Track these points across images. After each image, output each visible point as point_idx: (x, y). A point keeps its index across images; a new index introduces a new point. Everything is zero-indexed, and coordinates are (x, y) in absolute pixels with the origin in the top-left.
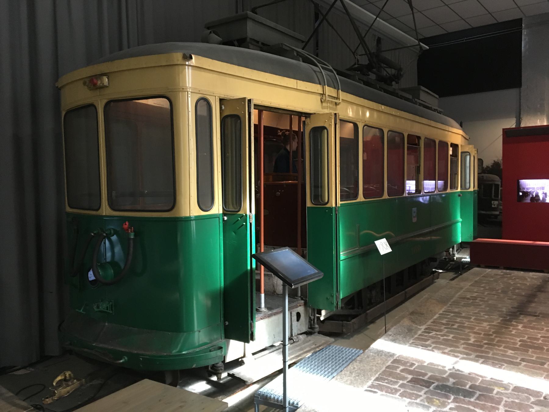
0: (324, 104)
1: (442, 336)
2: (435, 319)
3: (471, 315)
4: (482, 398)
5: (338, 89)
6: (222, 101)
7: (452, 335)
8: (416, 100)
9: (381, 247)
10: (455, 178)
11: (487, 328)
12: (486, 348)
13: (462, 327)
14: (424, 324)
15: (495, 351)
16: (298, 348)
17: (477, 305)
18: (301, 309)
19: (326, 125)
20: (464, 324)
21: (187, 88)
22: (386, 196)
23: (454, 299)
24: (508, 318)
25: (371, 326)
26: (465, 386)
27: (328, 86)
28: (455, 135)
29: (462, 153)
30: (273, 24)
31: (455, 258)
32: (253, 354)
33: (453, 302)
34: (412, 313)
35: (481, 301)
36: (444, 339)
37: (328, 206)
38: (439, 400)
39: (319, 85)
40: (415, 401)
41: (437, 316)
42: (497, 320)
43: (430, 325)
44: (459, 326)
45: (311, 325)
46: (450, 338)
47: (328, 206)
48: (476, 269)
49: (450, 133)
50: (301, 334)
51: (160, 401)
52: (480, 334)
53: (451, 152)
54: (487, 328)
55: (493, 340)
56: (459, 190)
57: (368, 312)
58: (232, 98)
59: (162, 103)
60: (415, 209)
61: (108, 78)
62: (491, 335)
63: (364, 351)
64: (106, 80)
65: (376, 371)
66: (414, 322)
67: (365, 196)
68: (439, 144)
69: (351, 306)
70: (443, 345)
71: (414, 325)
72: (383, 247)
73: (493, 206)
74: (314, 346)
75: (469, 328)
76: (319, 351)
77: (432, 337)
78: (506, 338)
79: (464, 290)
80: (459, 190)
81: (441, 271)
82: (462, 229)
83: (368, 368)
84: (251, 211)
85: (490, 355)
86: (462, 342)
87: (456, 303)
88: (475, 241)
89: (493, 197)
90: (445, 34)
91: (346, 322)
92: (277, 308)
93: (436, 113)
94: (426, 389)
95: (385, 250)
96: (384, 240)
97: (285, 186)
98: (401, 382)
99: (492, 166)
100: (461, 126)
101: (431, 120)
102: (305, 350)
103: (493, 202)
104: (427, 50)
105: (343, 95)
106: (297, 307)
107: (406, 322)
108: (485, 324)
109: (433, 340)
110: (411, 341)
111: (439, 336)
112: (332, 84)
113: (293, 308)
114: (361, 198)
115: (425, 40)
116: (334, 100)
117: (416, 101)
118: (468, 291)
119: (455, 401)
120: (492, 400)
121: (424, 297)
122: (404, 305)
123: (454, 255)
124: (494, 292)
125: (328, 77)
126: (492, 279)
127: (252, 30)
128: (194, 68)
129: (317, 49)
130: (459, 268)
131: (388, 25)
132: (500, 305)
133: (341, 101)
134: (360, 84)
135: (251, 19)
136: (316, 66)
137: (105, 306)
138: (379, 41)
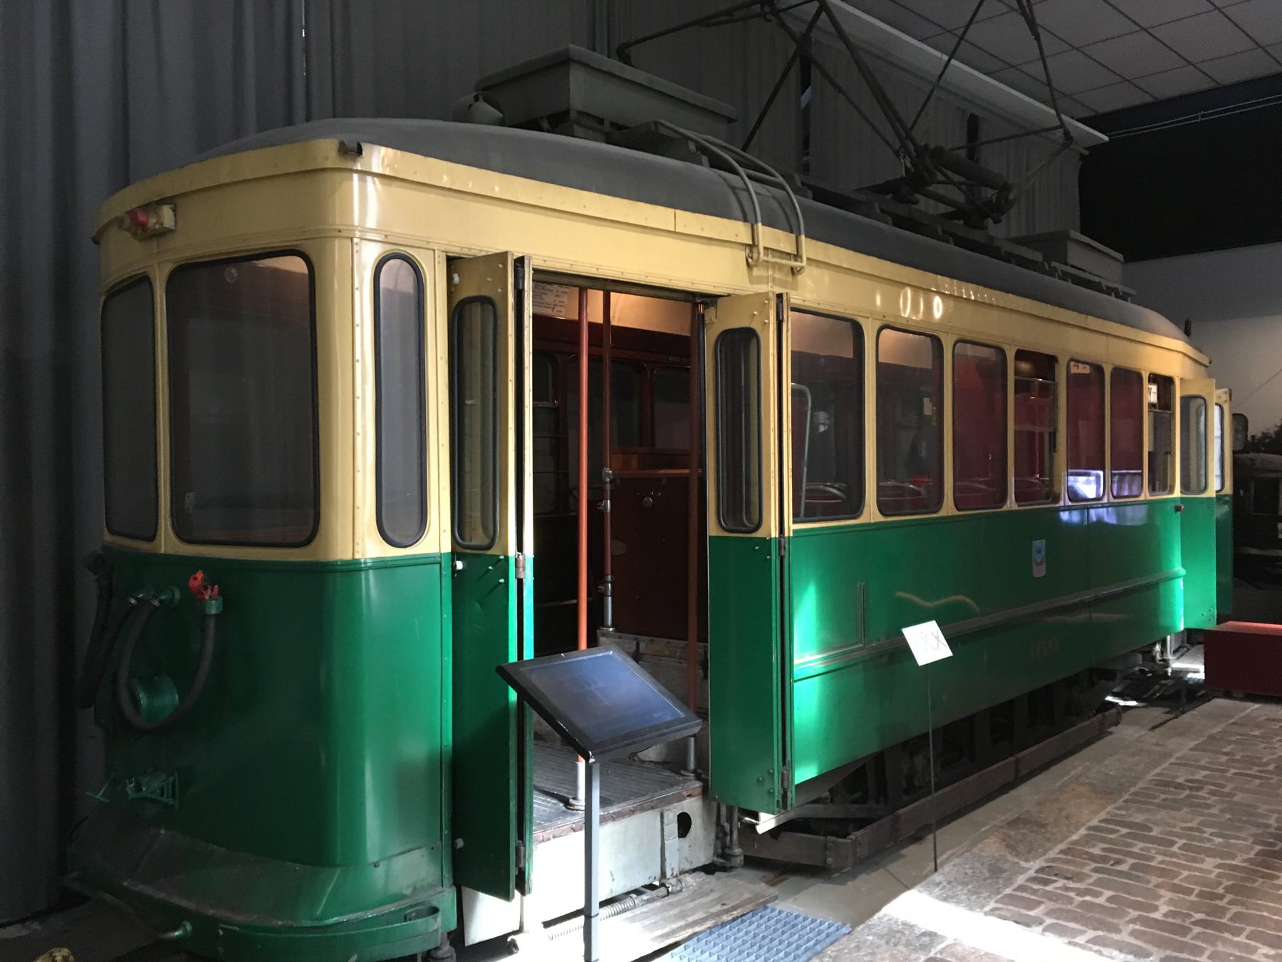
0: (756, 272)
1: (1081, 893)
2: (1075, 843)
3: (1177, 835)
6: (453, 263)
8: (1054, 264)
10: (1165, 463)
12: (1196, 937)
13: (1142, 868)
14: (1035, 858)
15: (1220, 948)
16: (676, 911)
17: (1199, 805)
18: (692, 806)
19: (755, 325)
20: (1151, 858)
21: (352, 228)
22: (948, 508)
23: (1141, 784)
25: (912, 850)
27: (807, 236)
28: (1166, 353)
29: (1182, 398)
31: (1170, 670)
32: (547, 924)
33: (1136, 794)
35: (1212, 793)
36: (1084, 905)
37: (759, 534)
41: (1083, 831)
42: (1246, 850)
43: (1054, 860)
44: (1133, 867)
45: (724, 847)
46: (1100, 901)
47: (759, 534)
48: (1220, 703)
49: (1149, 348)
52: (1189, 892)
53: (1153, 398)
54: (1212, 876)
55: (1222, 911)
56: (1177, 493)
57: (901, 812)
58: (474, 253)
59: (296, 265)
60: (1040, 544)
61: (174, 210)
62: (1221, 897)
63: (854, 926)
64: (167, 215)
66: (1012, 848)
67: (883, 508)
68: (1112, 375)
69: (856, 795)
70: (1075, 920)
71: (1010, 857)
72: (927, 643)
74: (718, 908)
75: (1162, 873)
76: (734, 920)
77: (1051, 897)
78: (1259, 908)
79: (1172, 760)
80: (1177, 493)
81: (1133, 703)
82: (1189, 594)
84: (520, 547)
86: (1134, 913)
87: (1141, 800)
88: (1231, 625)
90: (1146, 105)
91: (834, 838)
92: (625, 800)
93: (1113, 298)
96: (933, 625)
97: (664, 482)
99: (1277, 433)
100: (1187, 332)
101: (1087, 314)
102: (690, 919)
104: (1106, 144)
105: (810, 248)
106: (680, 798)
107: (992, 847)
108: (1209, 863)
109: (1052, 905)
110: (992, 905)
111: (1072, 894)
112: (736, 206)
113: (670, 803)
114: (871, 513)
115: (1093, 121)
116: (784, 262)
117: (1055, 268)
118: (1184, 763)
121: (1073, 773)
122: (1013, 793)
123: (1166, 663)
126: (1257, 733)
127: (581, 90)
128: (386, 181)
129: (807, 154)
130: (1182, 696)
131: (996, 83)
133: (804, 263)
134: (882, 225)
135: (579, 62)
136: (736, 173)
137: (156, 784)
138: (973, 126)
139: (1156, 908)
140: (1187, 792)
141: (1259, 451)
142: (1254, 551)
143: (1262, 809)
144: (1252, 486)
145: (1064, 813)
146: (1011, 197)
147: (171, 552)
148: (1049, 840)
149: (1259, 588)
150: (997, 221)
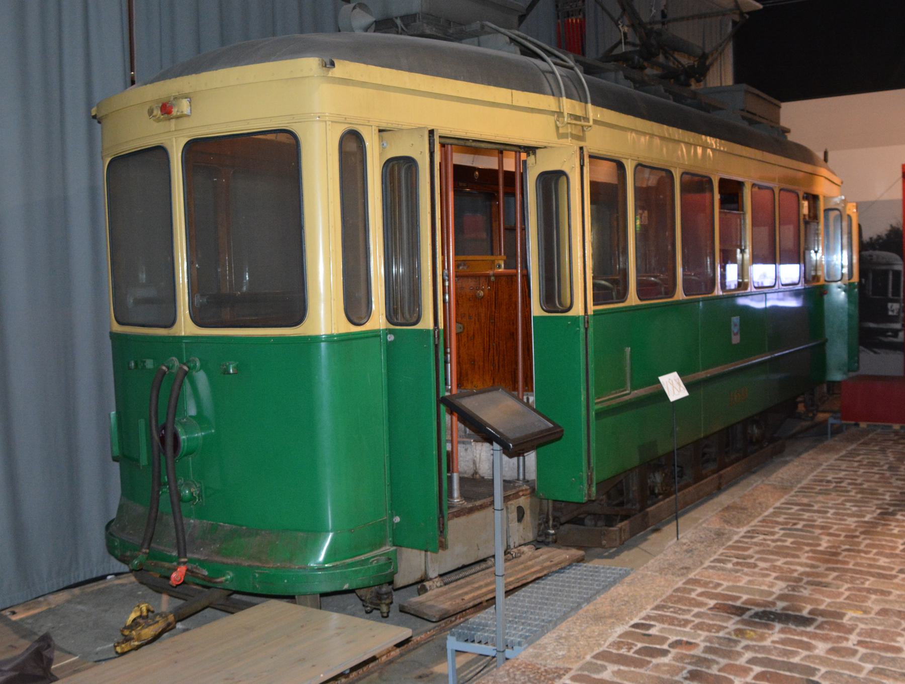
2: (768, 516)
4: (826, 626)
5: (586, 102)
7: (790, 540)
9: (670, 387)
11: (852, 527)
14: (744, 525)
24: (891, 509)
26: (800, 610)
27: (567, 97)
30: (518, 196)
34: (727, 509)
35: (850, 484)
37: (571, 313)
38: (754, 631)
39: (551, 97)
40: (717, 635)
41: (771, 510)
43: (755, 526)
44: (804, 526)
46: (787, 544)
50: (525, 544)
51: (302, 627)
52: (839, 536)
55: (859, 543)
57: (648, 509)
65: (655, 598)
66: (727, 522)
67: (641, 294)
71: (726, 527)
72: (674, 387)
73: (890, 313)
75: (822, 528)
83: (643, 593)
85: (851, 566)
86: (807, 548)
89: (890, 295)
94: (737, 618)
95: (676, 392)
98: (696, 610)
103: (890, 305)
104: (760, 11)
109: (757, 548)
119: (782, 631)
120: (840, 627)
124: (875, 469)
125: (566, 79)
132: (881, 490)
133: (591, 123)
139: (819, 545)
140: (834, 484)
141: (875, 249)
142: (872, 325)
143: (881, 490)
144: (871, 276)
145: (757, 501)
146: (708, 63)
147: (188, 334)
148: (750, 516)
149: (875, 353)
150: (698, 81)
